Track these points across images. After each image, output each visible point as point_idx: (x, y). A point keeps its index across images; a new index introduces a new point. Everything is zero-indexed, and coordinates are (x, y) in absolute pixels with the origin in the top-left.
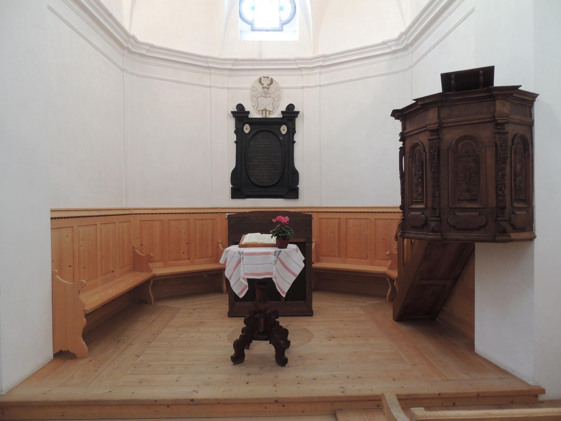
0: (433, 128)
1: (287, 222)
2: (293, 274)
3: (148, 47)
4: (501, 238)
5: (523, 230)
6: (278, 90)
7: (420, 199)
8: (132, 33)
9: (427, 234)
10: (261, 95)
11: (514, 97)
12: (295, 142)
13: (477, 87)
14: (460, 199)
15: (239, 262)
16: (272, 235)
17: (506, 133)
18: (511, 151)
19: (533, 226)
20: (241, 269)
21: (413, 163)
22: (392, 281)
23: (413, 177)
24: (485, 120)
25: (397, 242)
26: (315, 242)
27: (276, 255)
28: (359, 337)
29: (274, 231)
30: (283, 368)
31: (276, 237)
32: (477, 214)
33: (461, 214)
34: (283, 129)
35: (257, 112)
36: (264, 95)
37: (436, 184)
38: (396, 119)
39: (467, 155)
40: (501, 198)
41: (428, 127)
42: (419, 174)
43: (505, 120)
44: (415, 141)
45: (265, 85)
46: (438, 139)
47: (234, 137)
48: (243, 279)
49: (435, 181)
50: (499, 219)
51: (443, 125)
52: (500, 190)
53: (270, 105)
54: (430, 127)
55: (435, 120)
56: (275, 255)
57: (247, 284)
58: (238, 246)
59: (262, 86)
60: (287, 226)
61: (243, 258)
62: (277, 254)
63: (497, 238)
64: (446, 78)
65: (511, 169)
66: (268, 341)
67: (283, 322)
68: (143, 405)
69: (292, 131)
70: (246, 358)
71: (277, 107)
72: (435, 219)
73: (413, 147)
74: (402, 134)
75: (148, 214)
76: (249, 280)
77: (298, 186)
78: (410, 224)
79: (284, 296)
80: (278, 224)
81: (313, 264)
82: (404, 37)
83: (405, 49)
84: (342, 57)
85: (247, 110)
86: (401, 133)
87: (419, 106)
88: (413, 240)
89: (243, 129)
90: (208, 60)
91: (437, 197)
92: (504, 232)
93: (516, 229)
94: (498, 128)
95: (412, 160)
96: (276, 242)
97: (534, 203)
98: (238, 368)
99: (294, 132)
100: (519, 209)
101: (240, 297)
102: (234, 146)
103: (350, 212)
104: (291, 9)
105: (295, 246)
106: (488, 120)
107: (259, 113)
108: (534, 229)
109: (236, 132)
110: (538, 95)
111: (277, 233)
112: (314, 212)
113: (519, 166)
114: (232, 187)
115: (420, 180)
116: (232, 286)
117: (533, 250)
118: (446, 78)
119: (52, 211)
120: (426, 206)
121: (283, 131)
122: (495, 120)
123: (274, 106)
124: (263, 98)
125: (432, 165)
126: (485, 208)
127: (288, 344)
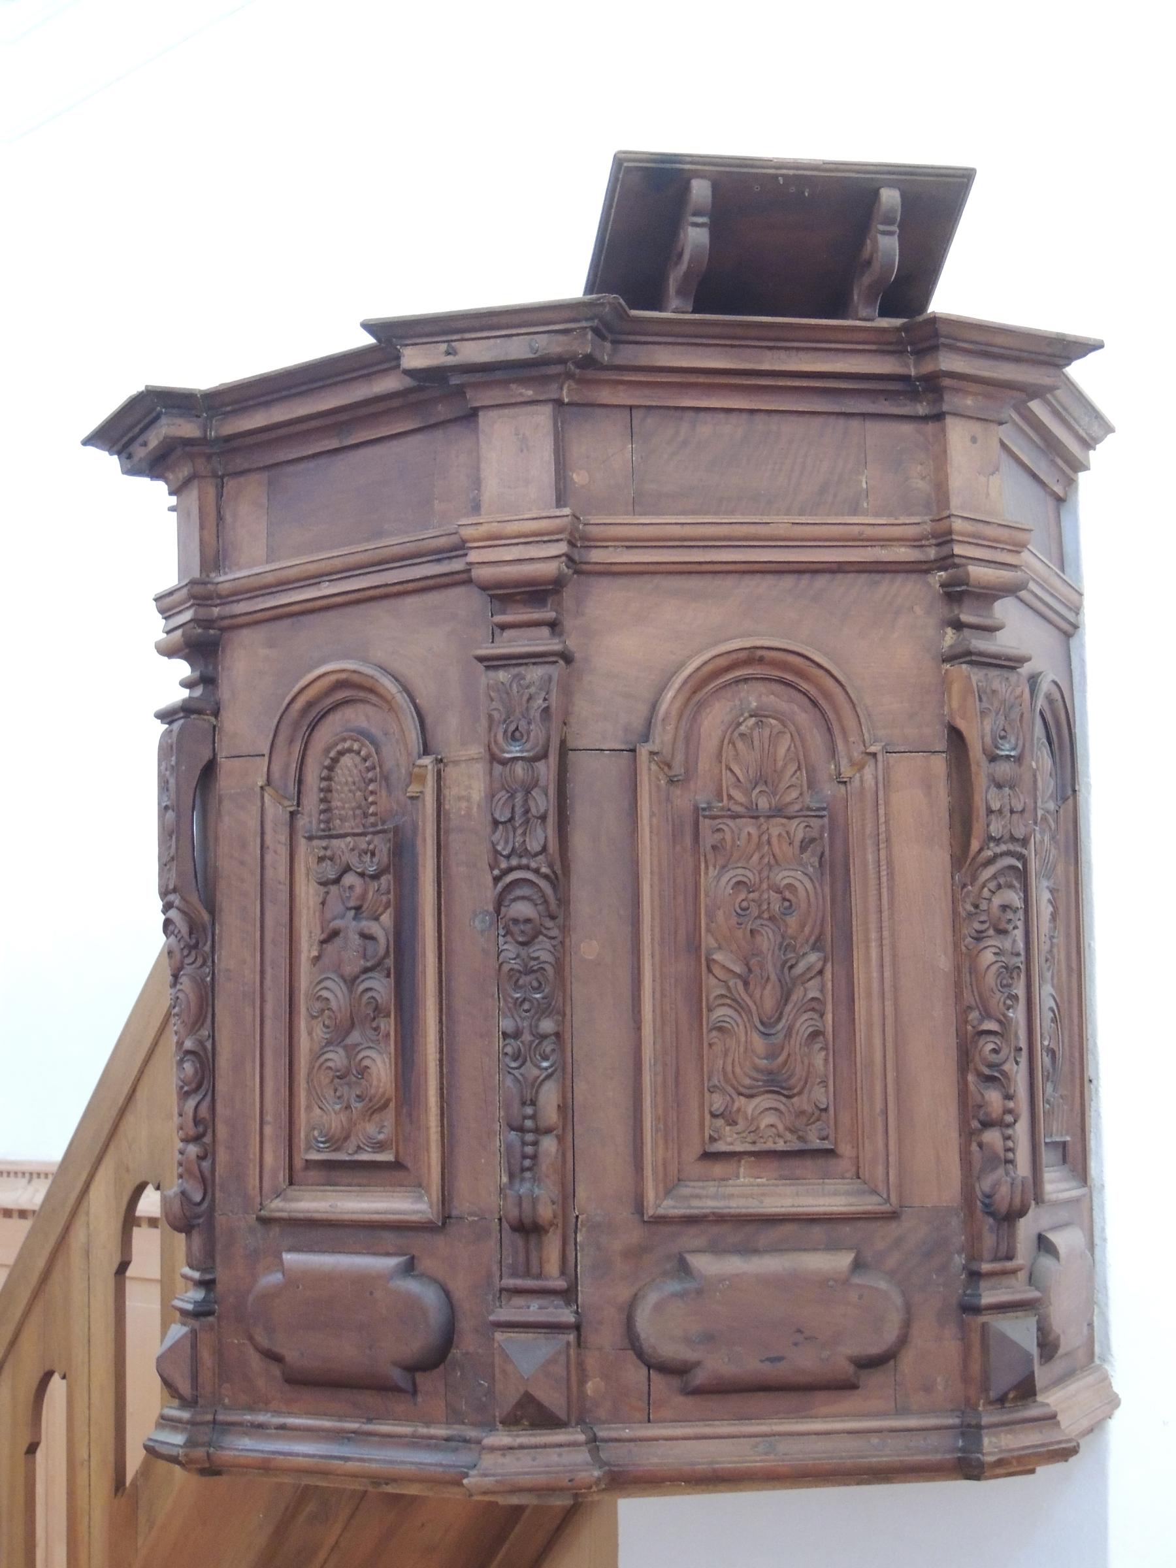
7: (380, 1146)
13: (837, 305)
14: (721, 1147)
21: (302, 846)
23: (307, 949)
32: (843, 1261)
33: (734, 1265)
39: (763, 804)
41: (473, 556)
42: (367, 937)
44: (323, 661)
50: (987, 1299)
51: (597, 555)
72: (534, 1310)
73: (310, 705)
78: (277, 1358)
91: (548, 1131)
119: (156, 600)
120: (445, 1199)
122: (946, 561)
125: (511, 870)
126: (893, 1216)
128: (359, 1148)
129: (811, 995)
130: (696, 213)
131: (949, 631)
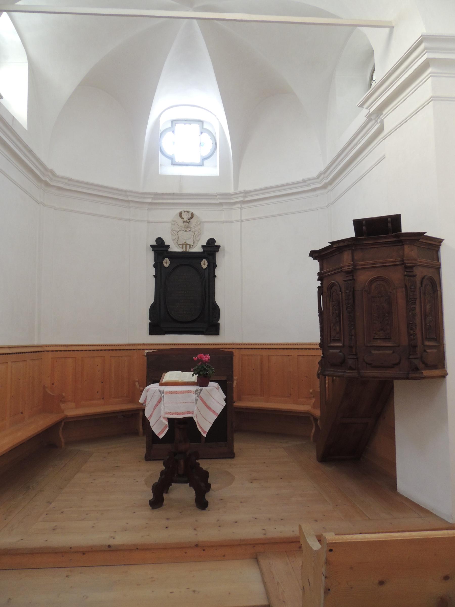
0: (348, 270)
1: (209, 360)
2: (214, 412)
3: (66, 181)
4: (414, 375)
5: (435, 367)
6: (199, 224)
7: (338, 338)
8: (50, 166)
9: (345, 372)
10: (181, 228)
11: (421, 242)
12: (216, 276)
14: (375, 338)
15: (160, 400)
16: (193, 373)
17: (415, 276)
18: (420, 293)
19: (444, 363)
20: (162, 408)
21: (330, 302)
22: (316, 419)
23: (331, 315)
24: (395, 263)
25: (319, 379)
26: (237, 380)
27: (197, 394)
28: (281, 479)
29: (195, 369)
30: (204, 512)
31: (197, 375)
32: (391, 352)
34: (204, 263)
35: (177, 246)
36: (185, 229)
37: (352, 323)
38: (313, 259)
40: (412, 337)
41: (343, 269)
43: (413, 263)
45: (185, 219)
46: (353, 280)
47: (153, 271)
48: (164, 418)
49: (351, 320)
50: (411, 357)
52: (411, 329)
53: (190, 239)
54: (345, 268)
55: (350, 262)
56: (196, 394)
57: (167, 423)
58: (158, 384)
59: (182, 220)
60: (208, 364)
61: (163, 396)
62: (198, 393)
63: (410, 376)
64: (358, 224)
65: (421, 310)
66: (188, 484)
67: (204, 464)
68: (56, 553)
69: (213, 265)
70: (165, 502)
71: (198, 241)
72: (352, 357)
74: (319, 274)
75: (60, 351)
76: (170, 420)
77: (219, 322)
79: (205, 435)
80: (200, 362)
81: (235, 402)
82: (322, 176)
83: (325, 187)
84: (263, 193)
85: (166, 243)
86: (318, 272)
87: (334, 249)
88: (334, 378)
89: (162, 263)
90: (128, 193)
92: (417, 369)
93: (428, 366)
94: (407, 270)
95: (330, 299)
96: (197, 380)
97: (444, 342)
98: (156, 512)
99: (215, 266)
100: (430, 347)
101: (159, 437)
102: (153, 279)
103: (272, 349)
104: (212, 145)
105: (216, 384)
106: (398, 263)
107: (179, 246)
108: (445, 366)
109: (155, 266)
110: (443, 240)
111: (198, 370)
112: (236, 348)
113: (428, 307)
114: (150, 323)
115: (337, 319)
116: (151, 426)
117: (446, 387)
118: (358, 224)
120: (344, 344)
121: (204, 265)
122: (404, 264)
123: (194, 240)
124: (184, 232)
126: (399, 346)
127: (208, 487)
128: (336, 338)
129: (387, 319)
130: (364, 225)
131: (406, 272)
